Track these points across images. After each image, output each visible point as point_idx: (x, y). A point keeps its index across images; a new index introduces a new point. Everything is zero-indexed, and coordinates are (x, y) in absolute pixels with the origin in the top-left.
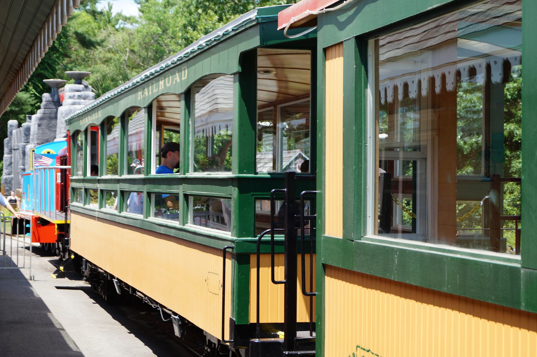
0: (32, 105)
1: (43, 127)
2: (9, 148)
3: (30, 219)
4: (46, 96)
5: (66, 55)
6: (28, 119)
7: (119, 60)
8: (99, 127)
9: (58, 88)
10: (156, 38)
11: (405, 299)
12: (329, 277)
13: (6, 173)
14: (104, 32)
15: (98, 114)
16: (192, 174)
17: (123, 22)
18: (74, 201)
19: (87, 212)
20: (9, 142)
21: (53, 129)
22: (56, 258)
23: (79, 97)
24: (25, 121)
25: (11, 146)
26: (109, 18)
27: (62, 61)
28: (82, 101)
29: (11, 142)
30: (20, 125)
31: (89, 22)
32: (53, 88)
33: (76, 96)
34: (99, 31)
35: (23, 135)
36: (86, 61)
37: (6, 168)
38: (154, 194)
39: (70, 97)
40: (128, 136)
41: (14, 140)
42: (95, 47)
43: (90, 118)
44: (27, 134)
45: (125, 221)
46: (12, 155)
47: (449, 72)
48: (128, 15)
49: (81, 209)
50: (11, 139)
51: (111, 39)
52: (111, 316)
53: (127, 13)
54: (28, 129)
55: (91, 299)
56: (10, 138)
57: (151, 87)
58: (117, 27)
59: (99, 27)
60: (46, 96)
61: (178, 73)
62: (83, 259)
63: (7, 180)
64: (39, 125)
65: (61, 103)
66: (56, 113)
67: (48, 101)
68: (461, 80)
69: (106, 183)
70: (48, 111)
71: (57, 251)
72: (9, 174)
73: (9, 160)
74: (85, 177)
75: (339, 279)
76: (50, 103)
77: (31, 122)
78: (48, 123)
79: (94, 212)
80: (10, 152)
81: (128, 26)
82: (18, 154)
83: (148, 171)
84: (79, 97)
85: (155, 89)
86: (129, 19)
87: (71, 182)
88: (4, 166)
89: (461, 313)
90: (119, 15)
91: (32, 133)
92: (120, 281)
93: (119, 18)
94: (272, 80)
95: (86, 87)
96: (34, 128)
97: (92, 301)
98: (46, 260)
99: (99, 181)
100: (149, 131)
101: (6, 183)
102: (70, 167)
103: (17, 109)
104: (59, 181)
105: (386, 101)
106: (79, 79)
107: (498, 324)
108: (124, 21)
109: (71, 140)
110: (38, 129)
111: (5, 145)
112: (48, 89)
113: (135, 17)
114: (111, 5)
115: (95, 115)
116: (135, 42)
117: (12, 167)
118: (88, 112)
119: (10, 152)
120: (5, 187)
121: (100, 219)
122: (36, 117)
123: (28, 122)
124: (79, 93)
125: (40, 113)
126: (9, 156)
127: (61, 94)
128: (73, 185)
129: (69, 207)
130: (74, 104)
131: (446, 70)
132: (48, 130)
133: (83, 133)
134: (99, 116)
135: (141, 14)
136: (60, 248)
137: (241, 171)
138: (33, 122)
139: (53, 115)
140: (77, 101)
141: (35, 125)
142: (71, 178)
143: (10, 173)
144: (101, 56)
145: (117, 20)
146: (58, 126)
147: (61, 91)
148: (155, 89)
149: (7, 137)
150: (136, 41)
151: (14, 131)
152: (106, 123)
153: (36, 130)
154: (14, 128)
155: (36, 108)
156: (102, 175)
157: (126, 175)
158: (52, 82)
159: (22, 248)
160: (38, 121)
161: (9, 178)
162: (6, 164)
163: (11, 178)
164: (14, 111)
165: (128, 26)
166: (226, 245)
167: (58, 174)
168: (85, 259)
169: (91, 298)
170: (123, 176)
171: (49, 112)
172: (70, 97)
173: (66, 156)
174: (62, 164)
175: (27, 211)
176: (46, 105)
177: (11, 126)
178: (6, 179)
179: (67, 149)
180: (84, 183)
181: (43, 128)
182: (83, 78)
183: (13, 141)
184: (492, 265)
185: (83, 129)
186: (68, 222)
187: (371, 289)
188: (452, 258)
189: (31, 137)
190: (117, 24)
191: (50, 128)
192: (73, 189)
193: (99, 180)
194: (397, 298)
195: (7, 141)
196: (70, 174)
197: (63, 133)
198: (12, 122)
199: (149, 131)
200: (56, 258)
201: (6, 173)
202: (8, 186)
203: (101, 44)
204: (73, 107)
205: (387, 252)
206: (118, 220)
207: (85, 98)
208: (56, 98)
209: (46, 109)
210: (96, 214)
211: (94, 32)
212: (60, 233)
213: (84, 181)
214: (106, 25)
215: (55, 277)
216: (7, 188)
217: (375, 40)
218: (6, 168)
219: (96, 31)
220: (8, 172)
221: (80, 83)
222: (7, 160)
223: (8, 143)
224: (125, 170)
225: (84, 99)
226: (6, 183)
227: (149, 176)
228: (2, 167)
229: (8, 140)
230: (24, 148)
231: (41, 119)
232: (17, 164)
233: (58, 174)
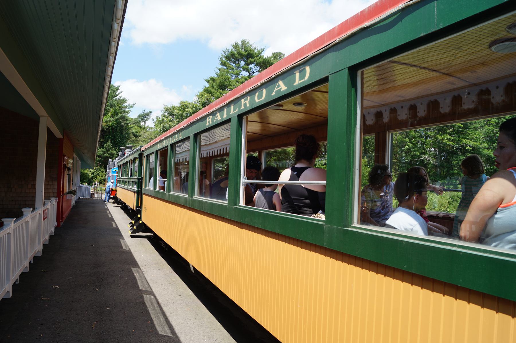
11: (297, 247)
12: (258, 233)
14: (143, 132)
24: (114, 160)
26: (144, 127)
30: (112, 161)
36: (133, 142)
40: (200, 146)
45: (122, 187)
47: (386, 111)
53: (150, 126)
54: (115, 162)
57: (177, 136)
60: (120, 152)
61: (219, 113)
68: (398, 114)
75: (210, 217)
80: (109, 169)
83: (128, 176)
85: (177, 138)
89: (302, 249)
105: (204, 156)
107: (276, 240)
112: (121, 150)
113: (153, 127)
119: (109, 169)
121: (121, 188)
127: (125, 152)
131: (183, 157)
135: (155, 127)
137: (138, 177)
144: (141, 140)
148: (177, 138)
151: (110, 163)
156: (133, 176)
158: (123, 148)
166: (135, 191)
172: (128, 153)
177: (110, 161)
184: (242, 209)
187: (278, 240)
188: (210, 203)
194: (287, 244)
198: (110, 160)
205: (200, 202)
208: (124, 153)
211: (139, 132)
221: (131, 149)
224: (123, 176)
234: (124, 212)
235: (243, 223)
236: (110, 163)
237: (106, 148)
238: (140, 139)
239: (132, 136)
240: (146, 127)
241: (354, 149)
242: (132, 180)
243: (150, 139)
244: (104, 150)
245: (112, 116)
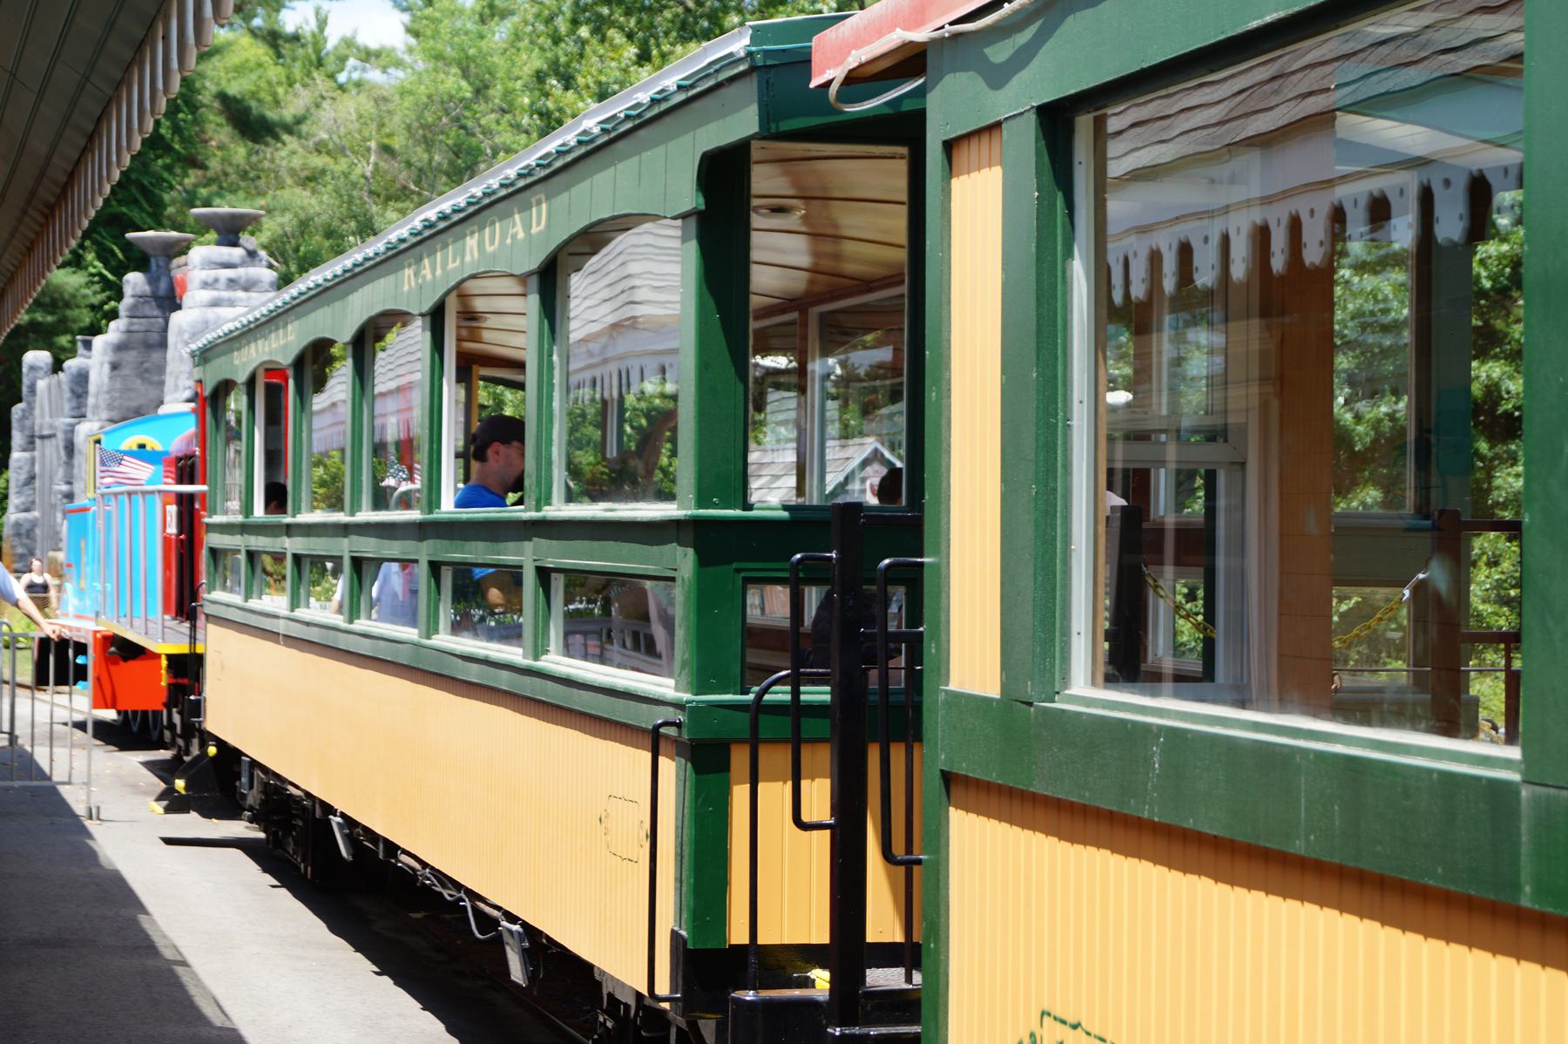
1: (125, 371)
3: (89, 640)
4: (134, 281)
5: (193, 162)
6: (80, 349)
7: (346, 175)
8: (290, 373)
9: (170, 257)
10: (455, 112)
11: (1182, 874)
12: (961, 809)
13: (17, 507)
14: (304, 92)
15: (286, 335)
17: (358, 63)
18: (217, 587)
19: (254, 620)
20: (27, 414)
21: (156, 378)
22: (165, 754)
23: (232, 284)
24: (72, 353)
26: (318, 51)
27: (182, 180)
28: (241, 294)
29: (32, 414)
30: (57, 367)
31: (260, 65)
32: (156, 256)
33: (223, 280)
34: (290, 90)
35: (67, 394)
37: (17, 493)
38: (450, 568)
39: (206, 285)
41: (42, 408)
42: (277, 138)
43: (264, 346)
44: (80, 390)
45: (365, 647)
46: (36, 453)
48: (373, 45)
49: (238, 611)
50: (31, 407)
52: (324, 925)
53: (370, 39)
54: (82, 378)
55: (267, 875)
56: (29, 403)
58: (342, 78)
59: (288, 78)
60: (134, 281)
62: (243, 758)
63: (21, 525)
64: (115, 367)
65: (178, 301)
66: (165, 329)
67: (141, 297)
69: (308, 535)
70: (139, 324)
71: (167, 734)
72: (27, 510)
73: (27, 468)
74: (247, 517)
75: (989, 816)
77: (89, 357)
78: (140, 360)
79: (275, 620)
80: (30, 444)
81: (374, 75)
82: (51, 452)
83: (433, 501)
84: (232, 284)
86: (378, 54)
87: (207, 532)
88: (12, 485)
89: (1345, 915)
90: (349, 43)
91: (92, 388)
92: (349, 822)
93: (346, 52)
95: (252, 254)
97: (269, 879)
98: (134, 761)
99: (289, 530)
100: (436, 383)
101: (18, 535)
102: (204, 488)
103: (50, 319)
104: (172, 530)
106: (230, 232)
107: (1454, 946)
108: (362, 61)
109: (208, 411)
110: (111, 378)
111: (15, 424)
112: (139, 259)
113: (393, 49)
114: (323, 13)
115: (277, 338)
116: (396, 123)
117: (34, 489)
118: (257, 327)
119: (30, 444)
120: (13, 547)
121: (292, 641)
122: (106, 343)
123: (82, 355)
124: (230, 273)
125: (118, 330)
126: (27, 455)
127: (177, 274)
128: (214, 540)
129: (201, 606)
130: (215, 303)
132: (139, 381)
133: (244, 389)
134: (290, 338)
135: (412, 41)
136: (175, 725)
137: (703, 501)
138: (96, 358)
139: (155, 337)
140: (225, 294)
141: (102, 364)
142: (206, 520)
143: (28, 505)
144: (296, 162)
145: (342, 60)
146: (169, 369)
147: (179, 267)
150: (397, 119)
151: (41, 385)
153: (106, 380)
154: (41, 374)
155: (104, 316)
156: (297, 511)
157: (367, 511)
158: (150, 239)
159: (66, 724)
160: (110, 353)
161: (27, 520)
162: (18, 480)
163: (31, 521)
164: (40, 324)
165: (374, 75)
166: (660, 715)
167: (169, 508)
168: (248, 756)
169: (265, 871)
170: (358, 514)
171: (143, 329)
172: (206, 285)
173: (192, 456)
174: (180, 481)
175: (78, 617)
176: (134, 307)
177: (32, 368)
178: (17, 524)
179: (196, 434)
180: (246, 536)
181: (126, 376)
182: (241, 229)
183: (37, 412)
184: (1435, 775)
185: (242, 377)
186: (200, 649)
187: (1082, 847)
188: (1320, 755)
189: (91, 400)
190: (342, 70)
191: (147, 375)
192: (214, 552)
193: (288, 526)
194: (1160, 871)
195: (20, 413)
196: (204, 507)
197: (185, 389)
198: (36, 357)
199: (436, 383)
200: (165, 754)
201: (17, 507)
202: (23, 545)
203: (295, 128)
204: (212, 313)
205: (1131, 736)
206: (344, 642)
207: (248, 286)
208: (163, 285)
209: (135, 320)
210: (281, 627)
211: (274, 95)
212: (174, 681)
213: (244, 529)
214: (309, 74)
215: (162, 811)
216: (20, 550)
217: (1095, 118)
218: (17, 493)
219: (280, 90)
220: (23, 503)
221: (235, 244)
222: (20, 468)
223: (24, 418)
224: (366, 498)
225: (246, 289)
226: (18, 535)
227: (435, 516)
228: (7, 488)
229: (23, 410)
230: (70, 431)
231: (120, 347)
232: (51, 479)
233: (169, 508)
234: (334, 929)
235: (966, 777)
238: (288, 154)
239: (219, 132)
240: (330, 45)
241: (1066, 315)
242: (293, 545)
243: (372, 159)
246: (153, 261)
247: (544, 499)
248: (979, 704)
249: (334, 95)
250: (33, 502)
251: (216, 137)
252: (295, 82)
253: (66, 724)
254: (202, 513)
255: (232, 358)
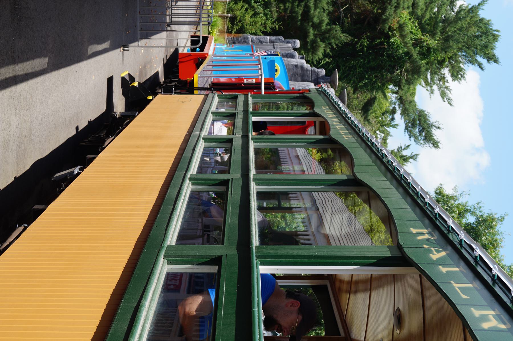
0: (312, 60)
1: (295, 69)
2: (275, 41)
3: (205, 51)
4: (323, 72)
5: (355, 90)
6: (301, 56)
8: (326, 137)
9: (330, 83)
13: (253, 38)
15: (346, 134)
16: (252, 146)
17: (382, 137)
18: (220, 99)
19: (202, 117)
20: (281, 41)
21: (293, 79)
22: (162, 79)
24: (299, 54)
25: (276, 43)
27: (350, 87)
29: (280, 42)
30: (295, 49)
31: (381, 108)
32: (330, 78)
34: (374, 117)
35: (287, 52)
37: (257, 38)
38: (216, 272)
41: (283, 45)
42: (364, 114)
43: (336, 122)
44: (288, 56)
46: (269, 44)
48: (388, 141)
49: (207, 109)
50: (283, 42)
51: (368, 127)
52: (44, 157)
53: (389, 140)
54: (292, 56)
55: (86, 124)
56: (284, 41)
58: (378, 132)
59: (377, 117)
60: (323, 72)
62: (138, 113)
63: (247, 39)
64: (296, 66)
65: (317, 85)
66: (308, 81)
67: (318, 74)
69: (242, 149)
70: (309, 73)
71: (169, 80)
72: (252, 41)
73: (264, 41)
74: (251, 113)
76: (316, 75)
77: (298, 59)
78: (298, 74)
79: (199, 129)
80: (271, 42)
83: (254, 114)
87: (245, 95)
88: (259, 37)
90: (388, 134)
91: (289, 59)
92: (74, 177)
93: (385, 133)
94: (350, 299)
96: (294, 62)
97: (83, 125)
98: (160, 69)
99: (245, 137)
100: (353, 261)
101: (244, 38)
102: (263, 93)
103: (309, 47)
104: (246, 81)
108: (383, 138)
109: (298, 95)
110: (292, 65)
111: (277, 37)
112: (330, 73)
114: (396, 126)
115: (342, 129)
117: (258, 43)
118: (343, 117)
119: (271, 42)
120: (241, 37)
122: (304, 64)
123: (299, 57)
125: (308, 67)
126: (268, 41)
128: (241, 98)
129: (212, 93)
132: (292, 74)
133: (311, 111)
134: (344, 136)
136: (171, 83)
138: (298, 60)
139: (306, 78)
141: (297, 62)
142: (250, 94)
143: (253, 41)
145: (383, 132)
146: (296, 82)
147: (327, 85)
149: (284, 39)
151: (290, 45)
152: (334, 146)
153: (292, 63)
154: (293, 45)
155: (312, 64)
156: (255, 140)
157: (256, 189)
159: (177, 45)
160: (300, 65)
161: (249, 41)
162: (261, 38)
163: (248, 42)
164: (307, 44)
167: (254, 80)
168: (138, 115)
169: (90, 123)
170: (254, 183)
171: (308, 75)
173: (275, 89)
174: (265, 84)
175: (214, 48)
176: (314, 71)
177: (294, 42)
178: (247, 38)
179: (283, 90)
180: (242, 113)
181: (293, 70)
183: (281, 44)
185: (317, 110)
186: (196, 92)
189: (286, 59)
190: (380, 132)
191: (294, 76)
192: (236, 97)
193: (247, 136)
195: (281, 39)
196: (255, 93)
198: (298, 43)
199: (353, 261)
200: (162, 79)
201: (253, 38)
202: (241, 40)
203: (366, 120)
206: (179, 174)
209: (311, 72)
210: (196, 133)
212: (188, 82)
213: (246, 111)
214: (379, 123)
215: (123, 75)
216: (240, 39)
218: (257, 38)
219: (374, 114)
220: (254, 40)
222: (264, 39)
223: (279, 40)
224: (264, 188)
227: (255, 260)
228: (258, 35)
229: (282, 40)
231: (302, 67)
232: (261, 48)
233: (254, 80)
236: (288, 42)
237: (328, 31)
244: (324, 27)
245: (417, 43)
246: (329, 77)
247: (259, 182)
248: (211, 288)
249: (373, 130)
250: (254, 43)
251: (360, 96)
252: (377, 119)
253: (177, 45)
254: (252, 93)
255: (325, 106)
